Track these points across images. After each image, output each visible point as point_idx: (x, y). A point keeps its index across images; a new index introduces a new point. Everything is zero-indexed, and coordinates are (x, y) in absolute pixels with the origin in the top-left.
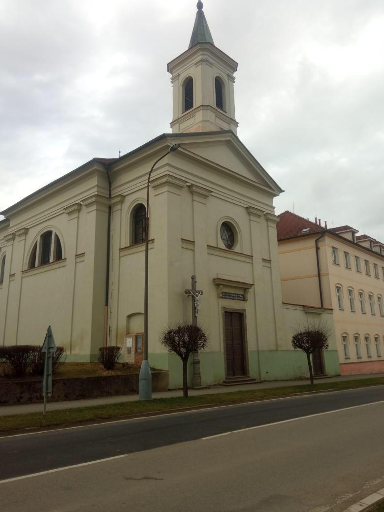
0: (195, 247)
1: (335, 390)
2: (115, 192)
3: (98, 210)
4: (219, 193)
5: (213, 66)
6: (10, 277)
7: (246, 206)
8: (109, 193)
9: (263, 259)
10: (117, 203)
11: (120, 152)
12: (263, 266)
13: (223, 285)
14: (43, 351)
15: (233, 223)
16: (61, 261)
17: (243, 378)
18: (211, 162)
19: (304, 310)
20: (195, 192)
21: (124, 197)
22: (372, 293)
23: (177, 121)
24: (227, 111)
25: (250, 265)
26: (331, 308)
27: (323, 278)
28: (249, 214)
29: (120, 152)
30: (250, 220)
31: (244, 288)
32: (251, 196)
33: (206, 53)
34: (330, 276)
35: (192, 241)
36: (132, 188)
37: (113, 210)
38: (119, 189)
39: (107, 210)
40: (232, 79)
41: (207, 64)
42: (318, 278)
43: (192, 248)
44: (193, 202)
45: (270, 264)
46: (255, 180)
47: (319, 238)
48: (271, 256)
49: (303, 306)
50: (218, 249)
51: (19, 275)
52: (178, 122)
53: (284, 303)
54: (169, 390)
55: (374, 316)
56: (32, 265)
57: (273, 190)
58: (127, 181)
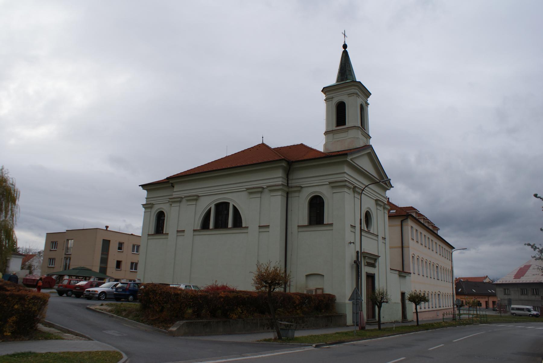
0: (356, 230)
1: (398, 334)
2: (293, 183)
3: (283, 196)
4: (369, 193)
5: (359, 97)
6: (177, 233)
7: (375, 199)
8: (286, 182)
9: (351, 225)
10: (295, 192)
11: (263, 137)
12: (351, 231)
13: (368, 257)
14: (145, 291)
15: (370, 212)
16: (241, 228)
17: (373, 320)
18: (364, 169)
19: (399, 274)
20: (379, 204)
21: (302, 187)
22: (414, 255)
23: (332, 132)
24: (366, 129)
25: (377, 241)
26: (409, 272)
27: (405, 250)
28: (377, 204)
29: (263, 137)
30: (377, 209)
31: (374, 258)
32: (376, 191)
33: (357, 88)
34: (410, 248)
35: (354, 226)
36: (306, 183)
37: (290, 196)
38: (293, 181)
39: (285, 195)
40: (367, 104)
41: (357, 96)
42: (400, 249)
43: (354, 231)
44: (377, 210)
45: (354, 229)
46: (378, 178)
47: (404, 220)
48: (386, 236)
49: (399, 271)
50: (364, 231)
51: (189, 232)
52: (332, 133)
53: (391, 269)
54: (347, 326)
55: (419, 275)
56: (205, 225)
57: (388, 187)
58: (303, 177)
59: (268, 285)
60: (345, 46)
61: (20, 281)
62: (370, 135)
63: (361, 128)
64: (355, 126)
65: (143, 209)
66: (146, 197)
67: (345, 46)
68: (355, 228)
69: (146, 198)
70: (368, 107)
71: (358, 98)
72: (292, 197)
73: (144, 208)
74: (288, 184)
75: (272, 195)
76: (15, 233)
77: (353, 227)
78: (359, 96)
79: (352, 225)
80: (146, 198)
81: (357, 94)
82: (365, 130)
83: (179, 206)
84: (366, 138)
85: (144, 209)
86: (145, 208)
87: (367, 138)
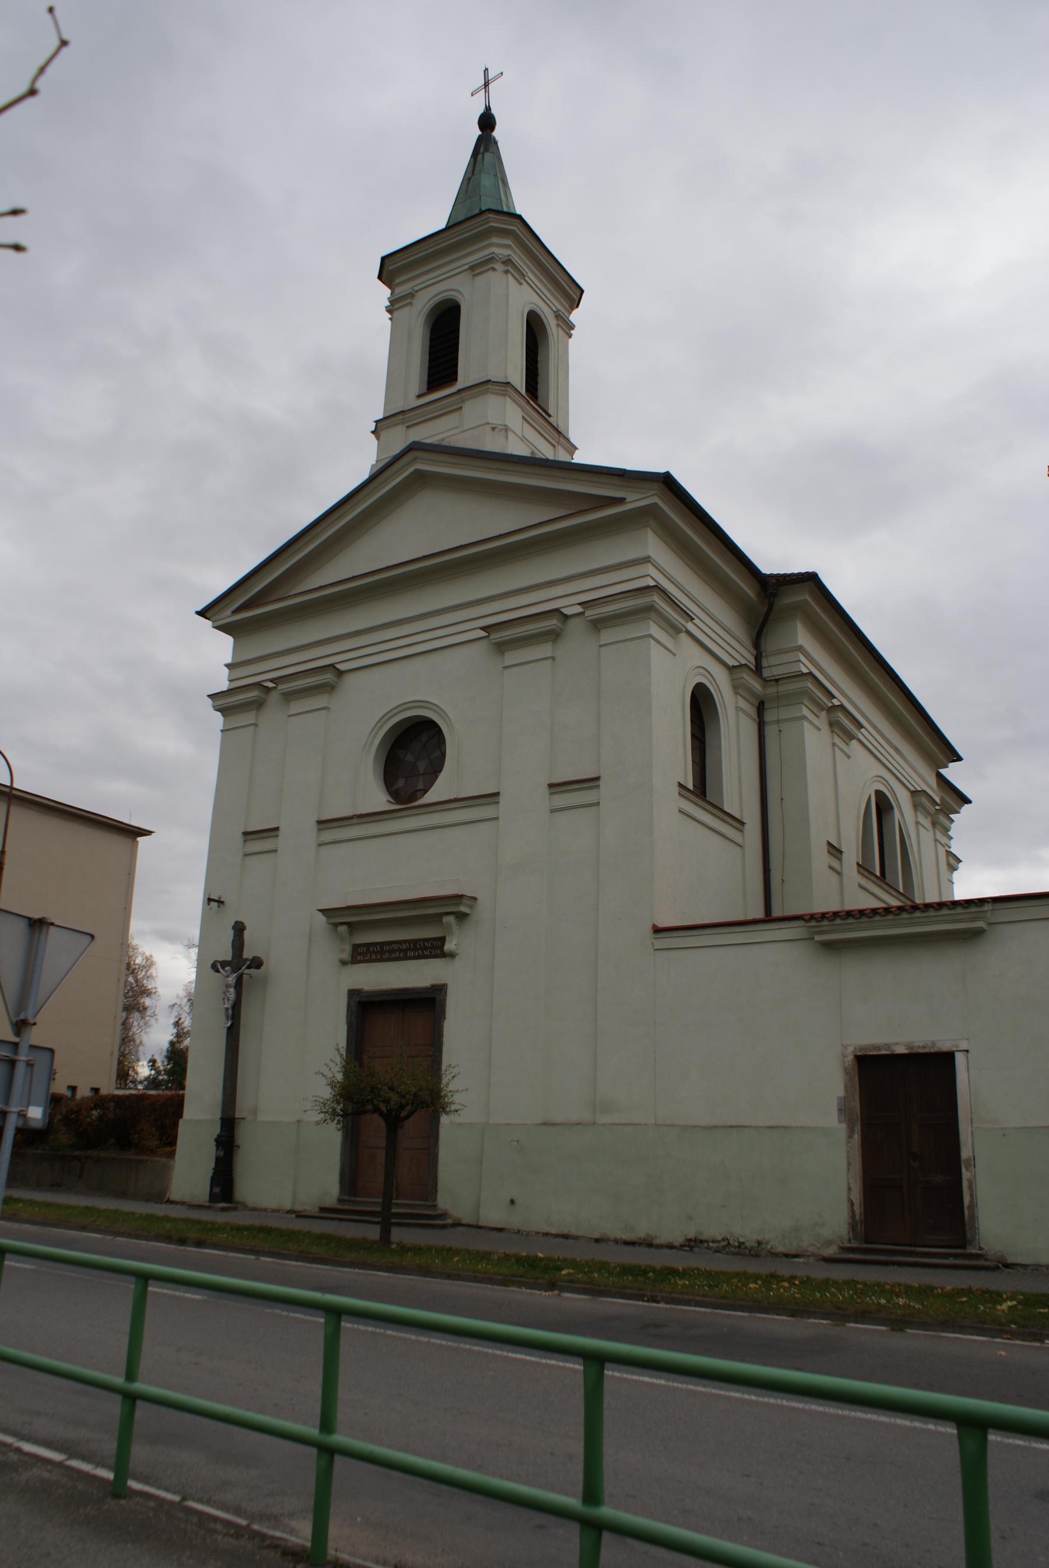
0: (844, 864)
5: (523, 281)
21: (340, 673)
24: (551, 412)
33: (509, 242)
41: (507, 272)
59: (581, 1275)
60: (487, 122)
61: (175, 1040)
62: (571, 440)
63: (525, 398)
64: (489, 381)
65: (218, 719)
66: (229, 660)
67: (487, 122)
68: (838, 855)
69: (227, 666)
70: (570, 336)
71: (511, 281)
72: (778, 707)
73: (219, 714)
74: (758, 658)
75: (291, 713)
76: (753, 719)
77: (835, 851)
78: (523, 276)
79: (830, 841)
80: (227, 666)
81: (508, 262)
82: (549, 416)
83: (255, 725)
84: (551, 448)
85: (218, 718)
86: (224, 711)
87: (554, 446)
